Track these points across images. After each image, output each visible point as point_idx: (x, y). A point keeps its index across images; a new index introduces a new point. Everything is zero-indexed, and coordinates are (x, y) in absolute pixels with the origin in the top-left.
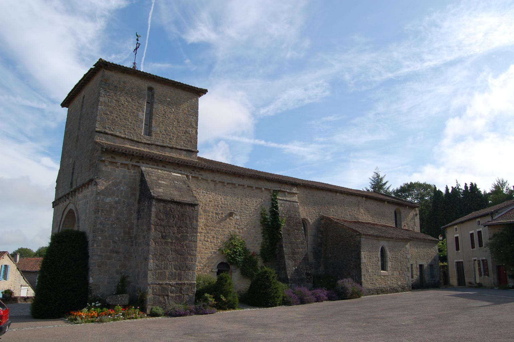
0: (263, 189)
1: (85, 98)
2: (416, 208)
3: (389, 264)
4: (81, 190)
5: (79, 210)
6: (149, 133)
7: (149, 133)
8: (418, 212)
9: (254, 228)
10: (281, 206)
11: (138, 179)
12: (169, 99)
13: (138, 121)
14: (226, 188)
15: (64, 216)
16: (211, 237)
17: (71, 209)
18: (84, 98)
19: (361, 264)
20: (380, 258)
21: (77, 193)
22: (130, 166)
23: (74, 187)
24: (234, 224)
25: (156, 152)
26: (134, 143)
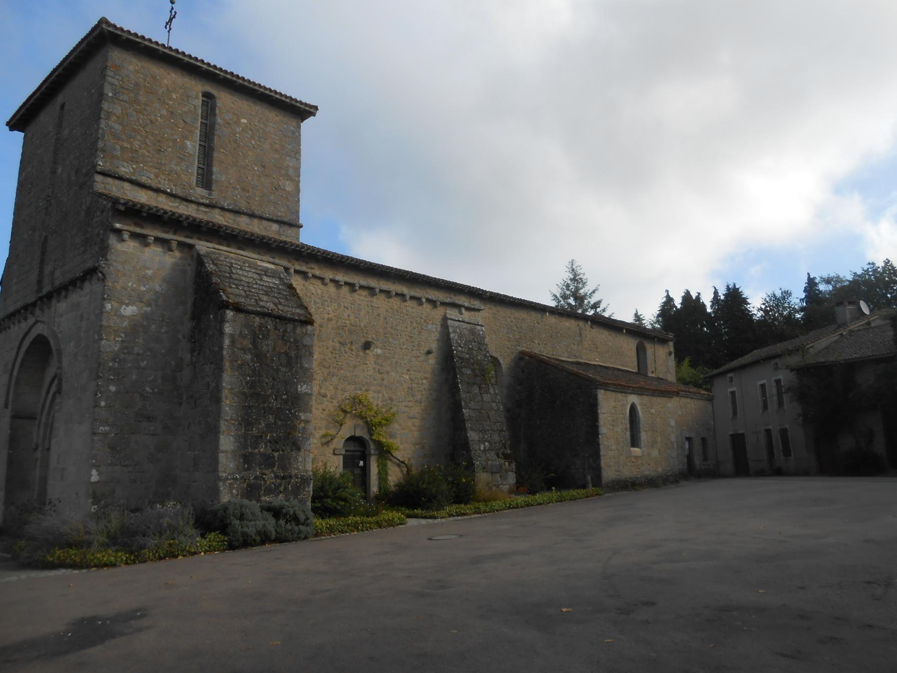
0: (424, 300)
1: (66, 107)
2: (670, 342)
3: (644, 436)
4: (63, 293)
5: (59, 335)
6: (206, 181)
7: (206, 181)
8: (672, 349)
9: (409, 373)
10: (454, 332)
11: (190, 271)
12: (244, 121)
13: (183, 157)
14: (356, 295)
15: (23, 350)
16: (332, 387)
17: (39, 335)
18: (62, 107)
19: (600, 436)
20: (629, 426)
21: (54, 302)
22: (174, 245)
23: (45, 291)
24: (372, 364)
25: (218, 218)
26: (178, 200)
